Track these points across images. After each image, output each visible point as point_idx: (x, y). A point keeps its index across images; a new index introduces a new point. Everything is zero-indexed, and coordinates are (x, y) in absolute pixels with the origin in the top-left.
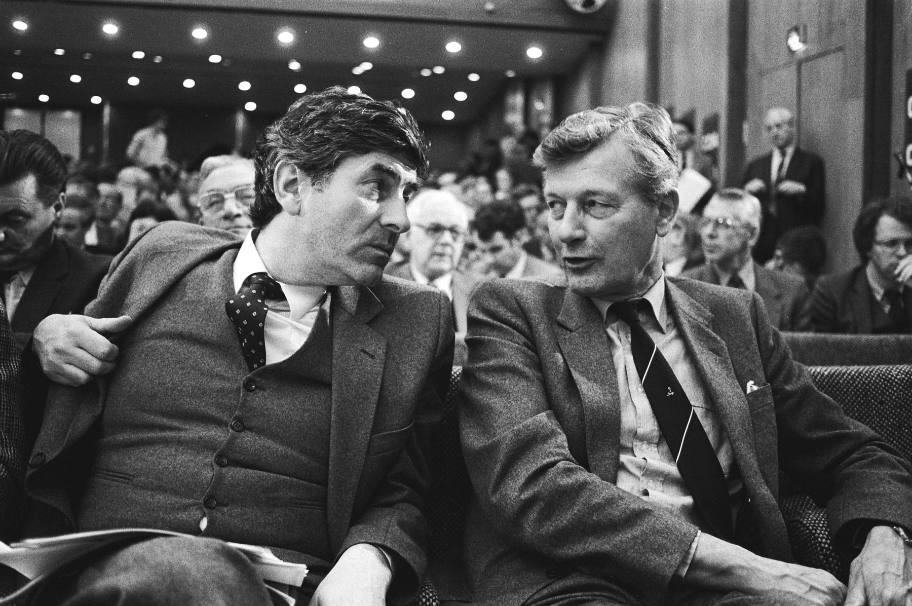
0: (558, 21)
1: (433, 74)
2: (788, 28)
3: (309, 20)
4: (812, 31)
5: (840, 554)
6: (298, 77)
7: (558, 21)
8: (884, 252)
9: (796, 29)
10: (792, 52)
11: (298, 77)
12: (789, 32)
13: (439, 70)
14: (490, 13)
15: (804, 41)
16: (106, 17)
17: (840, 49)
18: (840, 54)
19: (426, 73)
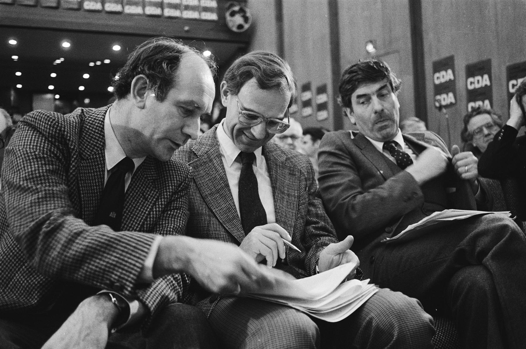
0: (222, 36)
1: (95, 65)
2: (366, 40)
3: (328, 46)
4: (379, 43)
5: (226, 108)
6: (17, 66)
7: (222, 36)
8: (450, 75)
9: (371, 42)
10: (368, 53)
11: (17, 66)
12: (367, 43)
13: (107, 61)
14: (187, 31)
15: (375, 47)
16: (7, 39)
17: (397, 51)
18: (396, 55)
19: (92, 64)
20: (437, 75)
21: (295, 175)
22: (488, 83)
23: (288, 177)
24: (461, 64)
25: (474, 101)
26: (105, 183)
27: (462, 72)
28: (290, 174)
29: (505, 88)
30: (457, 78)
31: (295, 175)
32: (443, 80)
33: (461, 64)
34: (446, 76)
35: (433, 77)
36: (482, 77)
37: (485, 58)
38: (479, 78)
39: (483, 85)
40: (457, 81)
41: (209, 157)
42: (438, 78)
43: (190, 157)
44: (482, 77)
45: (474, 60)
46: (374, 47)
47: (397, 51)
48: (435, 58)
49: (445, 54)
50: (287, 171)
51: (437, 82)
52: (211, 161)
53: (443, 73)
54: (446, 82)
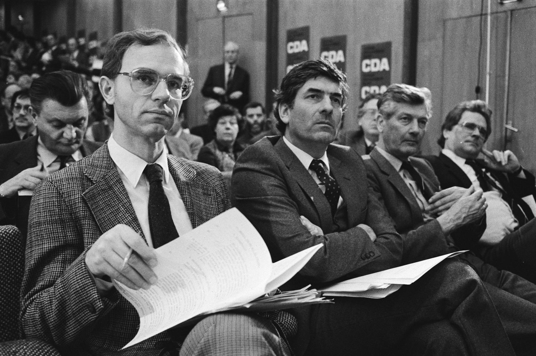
8: (384, 64)
10: (218, 11)
15: (227, 6)
17: (251, 14)
20: (290, 44)
21: (210, 195)
22: (387, 68)
23: (203, 198)
24: (316, 37)
25: (369, 85)
26: (508, 179)
27: (316, 44)
28: (204, 194)
29: (358, 65)
30: (311, 49)
31: (210, 195)
32: (296, 50)
33: (316, 37)
34: (299, 46)
35: (286, 46)
36: (381, 60)
37: (340, 34)
38: (377, 61)
39: (381, 69)
40: (311, 52)
41: (107, 183)
42: (292, 47)
43: (83, 184)
44: (381, 60)
45: (329, 34)
46: (225, 6)
47: (251, 14)
48: (290, 26)
49: (301, 24)
50: (201, 191)
51: (290, 51)
52: (111, 188)
53: (297, 43)
54: (299, 53)
